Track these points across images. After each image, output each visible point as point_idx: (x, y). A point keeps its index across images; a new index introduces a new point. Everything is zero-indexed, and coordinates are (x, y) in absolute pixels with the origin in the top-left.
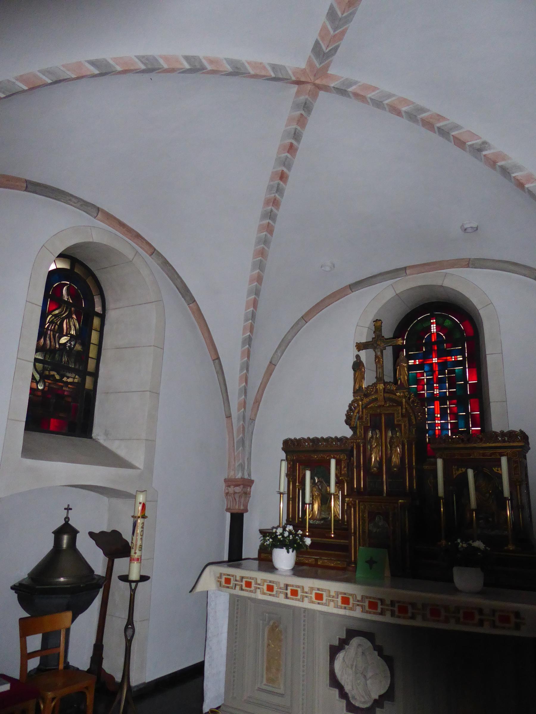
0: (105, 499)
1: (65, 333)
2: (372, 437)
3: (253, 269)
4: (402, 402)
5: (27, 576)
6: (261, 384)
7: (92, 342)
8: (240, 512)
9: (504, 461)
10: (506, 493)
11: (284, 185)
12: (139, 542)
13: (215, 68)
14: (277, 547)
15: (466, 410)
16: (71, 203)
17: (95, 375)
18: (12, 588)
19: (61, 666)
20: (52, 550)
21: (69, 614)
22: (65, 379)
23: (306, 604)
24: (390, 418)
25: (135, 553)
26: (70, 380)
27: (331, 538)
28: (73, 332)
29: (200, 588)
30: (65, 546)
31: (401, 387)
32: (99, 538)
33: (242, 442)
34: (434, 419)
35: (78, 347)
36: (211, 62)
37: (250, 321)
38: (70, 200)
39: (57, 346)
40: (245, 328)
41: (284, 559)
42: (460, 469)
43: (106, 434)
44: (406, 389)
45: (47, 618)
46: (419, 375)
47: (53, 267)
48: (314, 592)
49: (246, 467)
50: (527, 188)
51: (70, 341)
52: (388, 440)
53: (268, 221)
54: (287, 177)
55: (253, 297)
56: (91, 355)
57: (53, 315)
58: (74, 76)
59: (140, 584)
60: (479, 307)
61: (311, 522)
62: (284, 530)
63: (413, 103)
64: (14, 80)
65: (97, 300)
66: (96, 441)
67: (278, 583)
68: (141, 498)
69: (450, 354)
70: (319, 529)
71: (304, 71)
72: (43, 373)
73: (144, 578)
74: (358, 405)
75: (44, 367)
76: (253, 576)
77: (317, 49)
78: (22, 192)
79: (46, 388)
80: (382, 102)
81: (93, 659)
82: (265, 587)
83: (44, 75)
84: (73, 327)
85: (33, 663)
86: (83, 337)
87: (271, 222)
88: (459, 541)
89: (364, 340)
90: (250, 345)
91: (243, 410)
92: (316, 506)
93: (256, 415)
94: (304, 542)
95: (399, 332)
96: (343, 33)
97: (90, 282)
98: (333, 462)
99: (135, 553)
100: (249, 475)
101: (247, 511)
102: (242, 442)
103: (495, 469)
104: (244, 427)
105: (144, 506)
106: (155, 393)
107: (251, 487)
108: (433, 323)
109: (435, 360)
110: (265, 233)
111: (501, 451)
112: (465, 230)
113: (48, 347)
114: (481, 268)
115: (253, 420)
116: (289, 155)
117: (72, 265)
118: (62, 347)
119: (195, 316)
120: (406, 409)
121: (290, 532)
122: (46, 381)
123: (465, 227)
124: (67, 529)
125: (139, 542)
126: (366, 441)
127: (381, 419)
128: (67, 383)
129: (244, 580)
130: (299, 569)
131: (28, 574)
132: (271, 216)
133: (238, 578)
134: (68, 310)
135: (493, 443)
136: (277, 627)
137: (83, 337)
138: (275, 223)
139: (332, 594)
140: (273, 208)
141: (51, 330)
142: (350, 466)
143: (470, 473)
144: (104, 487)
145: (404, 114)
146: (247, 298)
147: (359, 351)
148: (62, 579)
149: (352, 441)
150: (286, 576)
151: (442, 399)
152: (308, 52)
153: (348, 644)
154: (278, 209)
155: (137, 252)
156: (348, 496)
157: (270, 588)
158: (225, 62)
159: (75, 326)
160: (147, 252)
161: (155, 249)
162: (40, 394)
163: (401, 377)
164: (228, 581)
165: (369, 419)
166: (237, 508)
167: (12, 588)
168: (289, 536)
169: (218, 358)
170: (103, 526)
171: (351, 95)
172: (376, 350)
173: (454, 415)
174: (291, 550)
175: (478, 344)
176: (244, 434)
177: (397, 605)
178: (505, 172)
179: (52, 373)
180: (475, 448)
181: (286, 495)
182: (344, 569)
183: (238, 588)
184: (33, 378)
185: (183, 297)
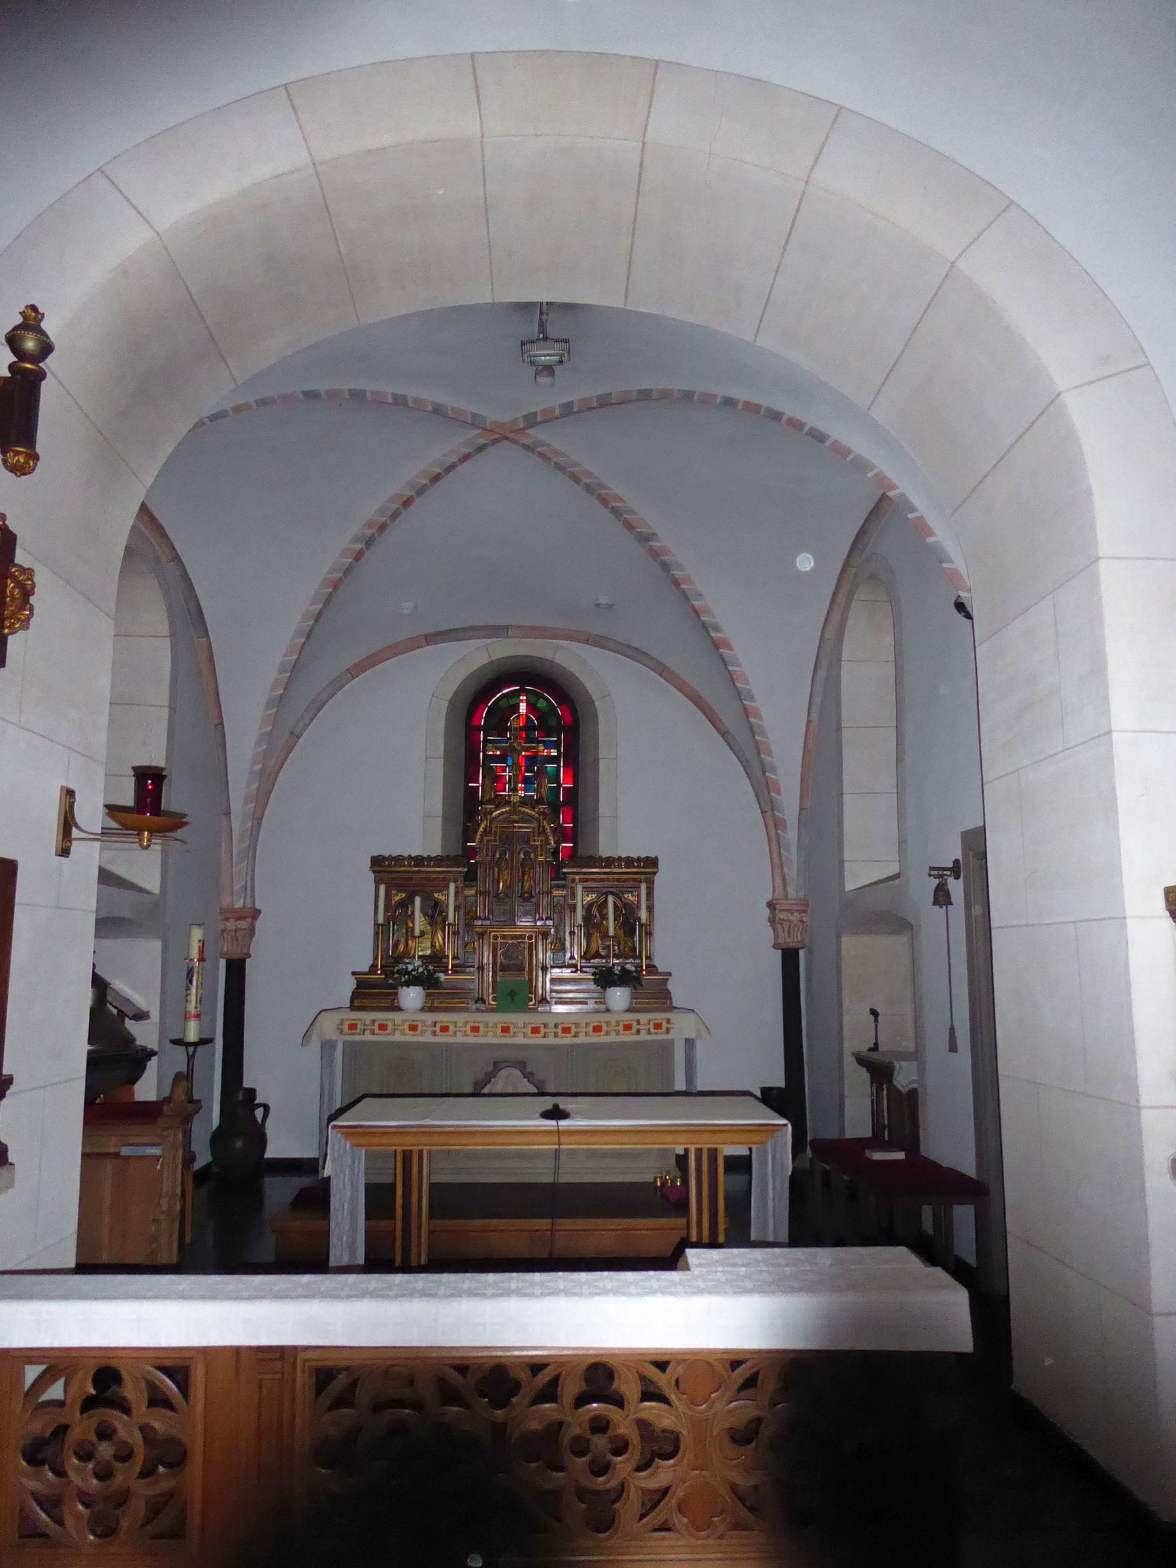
59: (200, 1048)
77: (727, 732)
101: (249, 956)
108: (522, 701)
164: (353, 1027)
166: (236, 953)
178: (665, 566)
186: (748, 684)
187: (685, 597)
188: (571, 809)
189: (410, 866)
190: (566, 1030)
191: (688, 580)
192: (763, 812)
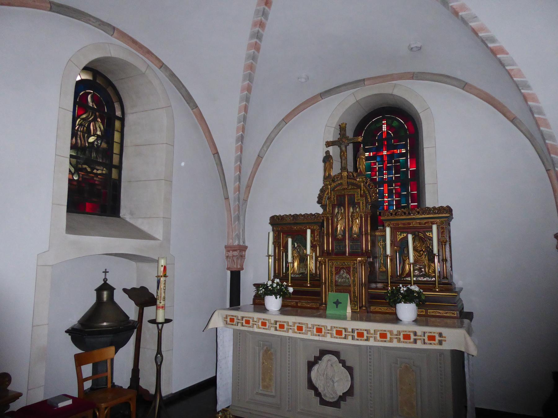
0: (133, 263)
1: (92, 134)
2: (338, 212)
3: (244, 80)
4: (361, 186)
7: (115, 140)
8: (237, 270)
9: (435, 227)
10: (435, 251)
11: (268, 10)
12: (163, 295)
14: (268, 295)
15: (407, 190)
17: (119, 168)
18: (66, 332)
19: (109, 385)
20: (95, 304)
21: (113, 348)
22: (95, 171)
23: (290, 334)
24: (352, 197)
25: (160, 303)
26: (99, 172)
27: (308, 287)
28: (99, 133)
29: (211, 326)
30: (105, 299)
31: (360, 174)
32: (132, 293)
33: (238, 218)
34: (383, 197)
38: (90, 20)
39: (87, 145)
40: (238, 128)
41: (273, 303)
43: (132, 214)
44: (364, 175)
45: (96, 352)
47: (79, 78)
48: (296, 325)
49: (241, 237)
50: (451, 6)
51: (97, 140)
52: (350, 214)
55: (244, 103)
56: (115, 152)
57: (82, 119)
59: (165, 325)
60: (419, 111)
61: (292, 276)
62: (273, 281)
65: (117, 106)
66: (124, 220)
67: (269, 320)
68: (162, 262)
69: (396, 147)
70: (299, 280)
72: (77, 166)
73: (168, 321)
75: (77, 161)
76: (267, 318)
77: (515, 118)
78: (46, 12)
79: (80, 179)
81: (132, 380)
82: (260, 324)
84: (98, 129)
85: (88, 385)
86: (107, 136)
88: (401, 285)
89: (331, 140)
90: (242, 142)
92: (296, 264)
93: (248, 197)
94: (288, 291)
95: (357, 132)
97: (110, 90)
98: (309, 231)
99: (160, 303)
100: (244, 242)
101: (243, 269)
103: (428, 234)
104: (239, 207)
105: (165, 267)
106: (169, 181)
107: (245, 251)
109: (385, 153)
111: (432, 220)
112: (412, 49)
113: (79, 145)
115: (246, 201)
117: (94, 76)
119: (198, 119)
120: (364, 190)
121: (278, 284)
124: (105, 287)
125: (163, 295)
126: (333, 216)
128: (97, 175)
129: (244, 319)
130: (284, 310)
132: (258, 36)
133: (240, 318)
136: (269, 351)
137: (107, 136)
138: (261, 42)
141: (80, 131)
142: (321, 235)
143: (410, 237)
148: (105, 324)
150: (275, 315)
151: (390, 182)
153: (320, 360)
154: (263, 30)
155: (148, 65)
156: (320, 256)
157: (264, 324)
159: (100, 128)
160: (155, 65)
161: (163, 63)
162: (75, 183)
164: (232, 320)
165: (335, 198)
166: (235, 267)
167: (66, 332)
168: (277, 287)
169: (217, 153)
170: (134, 284)
173: (398, 195)
174: (278, 297)
175: (418, 140)
176: (239, 211)
177: (356, 332)
179: (84, 166)
180: (414, 219)
181: (273, 257)
182: (318, 309)
183: (240, 324)
184: (70, 171)
185: (188, 103)
186: (524, 77)
187: (464, 22)
188: (412, 182)
190: (361, 335)
192: (547, 170)
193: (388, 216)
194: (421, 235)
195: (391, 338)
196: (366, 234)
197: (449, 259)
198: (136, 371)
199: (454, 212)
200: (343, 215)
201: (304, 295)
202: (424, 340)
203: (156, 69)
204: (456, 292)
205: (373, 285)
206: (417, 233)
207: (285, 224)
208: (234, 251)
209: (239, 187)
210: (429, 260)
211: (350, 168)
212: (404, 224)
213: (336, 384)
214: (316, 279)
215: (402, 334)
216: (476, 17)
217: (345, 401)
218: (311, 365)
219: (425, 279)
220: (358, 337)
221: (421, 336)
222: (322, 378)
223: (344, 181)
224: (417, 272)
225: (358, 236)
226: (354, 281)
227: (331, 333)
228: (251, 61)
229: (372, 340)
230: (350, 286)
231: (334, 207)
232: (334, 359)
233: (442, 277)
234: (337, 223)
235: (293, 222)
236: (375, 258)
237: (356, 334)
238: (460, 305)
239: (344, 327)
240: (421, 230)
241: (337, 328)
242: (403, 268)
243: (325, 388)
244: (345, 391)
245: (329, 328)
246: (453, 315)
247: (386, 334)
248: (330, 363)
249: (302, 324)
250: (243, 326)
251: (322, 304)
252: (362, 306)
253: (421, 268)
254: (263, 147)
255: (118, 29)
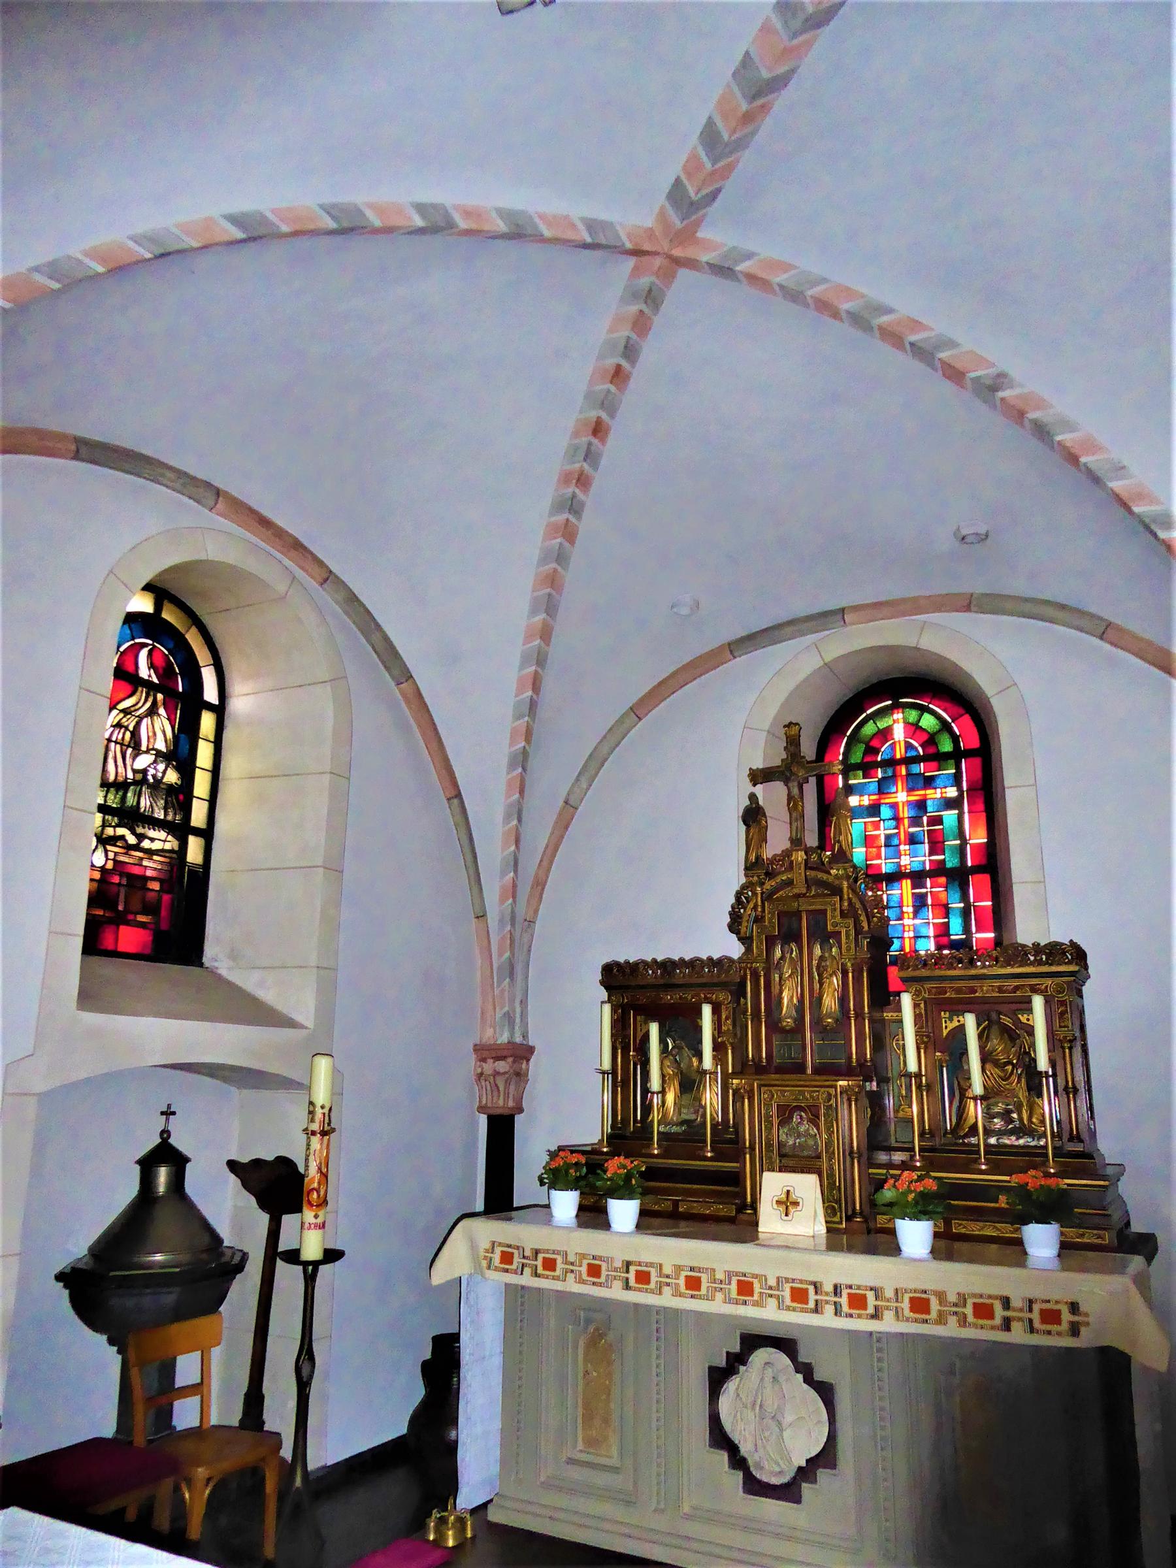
1: (144, 748)
2: (782, 958)
3: (534, 612)
5: (86, 1252)
6: (547, 846)
8: (506, 1112)
9: (1038, 1002)
10: (1043, 1064)
11: (601, 446)
13: (474, 226)
16: (165, 482)
18: (60, 1277)
22: (146, 844)
23: (667, 1300)
26: (157, 846)
27: (706, 1159)
32: (250, 1173)
33: (510, 970)
35: (172, 777)
36: (467, 213)
37: (526, 718)
38: (163, 475)
40: (514, 733)
42: (955, 1018)
43: (234, 955)
46: (870, 827)
49: (518, 1020)
50: (1085, 464)
52: (815, 963)
53: (565, 516)
54: (607, 431)
57: (121, 711)
58: (195, 244)
61: (662, 1129)
63: (863, 296)
64: (80, 257)
66: (213, 973)
71: (650, 233)
73: (332, 1256)
74: (755, 894)
79: (110, 865)
80: (802, 292)
83: (140, 245)
86: (181, 755)
87: (572, 519)
91: (510, 901)
92: (670, 1097)
93: (536, 911)
96: (730, 168)
97: (194, 639)
98: (707, 1010)
100: (525, 1036)
101: (520, 1110)
102: (510, 970)
107: (528, 1060)
110: (559, 540)
114: (993, 613)
116: (613, 388)
117: (158, 607)
118: (139, 777)
120: (850, 900)
122: (109, 848)
123: (964, 532)
124: (165, 1154)
127: (800, 919)
128: (150, 853)
129: (540, 1256)
131: (91, 1249)
134: (151, 699)
135: (1020, 966)
136: (601, 1336)
137: (181, 755)
139: (720, 1275)
140: (577, 491)
141: (116, 742)
142: (738, 1014)
144: (241, 1069)
145: (844, 315)
146: (520, 669)
147: (754, 785)
148: (159, 1257)
149: (743, 965)
151: (917, 877)
152: (661, 199)
153: (744, 1363)
155: (294, 577)
158: (494, 214)
159: (164, 732)
163: (842, 838)
166: (502, 1104)
167: (60, 1277)
169: (459, 795)
171: (740, 276)
172: (790, 785)
177: (845, 1292)
178: (1042, 432)
179: (121, 831)
183: (527, 1271)
189: (984, 966)
190: (858, 1301)
191: (1093, 447)
193: (916, 968)
194: (1006, 1020)
195: (940, 1313)
196: (859, 1016)
197: (1081, 1086)
198: (254, 1400)
199: (1090, 961)
200: (797, 965)
201: (698, 1187)
202: (1031, 1321)
203: (312, 584)
204: (1103, 1177)
205: (882, 1157)
206: (994, 1016)
207: (643, 987)
208: (497, 1058)
209: (514, 886)
210: (1029, 1089)
211: (812, 840)
212: (958, 991)
213: (786, 1434)
214: (729, 1140)
215: (970, 1302)
216: (1123, 468)
217: (814, 1481)
218: (718, 1378)
219: (1021, 1142)
220: (851, 1306)
221: (1021, 1310)
222: (750, 1415)
223: (799, 875)
224: (998, 1123)
225: (837, 1021)
226: (829, 1144)
227: (778, 1297)
228: (554, 565)
229: (888, 1315)
230: (819, 1157)
231: (770, 942)
232: (783, 1360)
233: (1066, 1137)
234: (781, 985)
235: (662, 982)
236: (883, 1080)
237: (844, 1300)
238: (1116, 1216)
239: (811, 1279)
240: (1004, 1008)
241: (793, 1280)
242: (961, 1112)
243: (759, 1443)
244: (813, 1454)
245: (772, 1282)
246: (1099, 1241)
247: (928, 1300)
248: (769, 1372)
249: (699, 1270)
250: (536, 1275)
251: (742, 1208)
252: (854, 1214)
253: (1009, 1112)
254: (577, 780)
255: (227, 495)
